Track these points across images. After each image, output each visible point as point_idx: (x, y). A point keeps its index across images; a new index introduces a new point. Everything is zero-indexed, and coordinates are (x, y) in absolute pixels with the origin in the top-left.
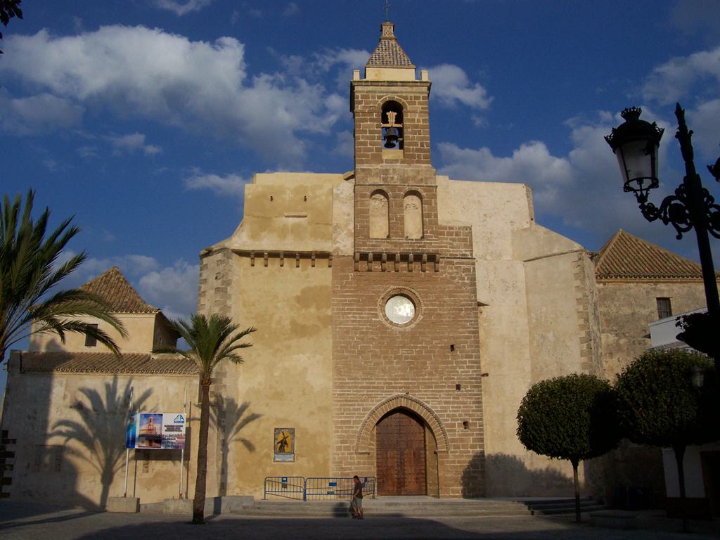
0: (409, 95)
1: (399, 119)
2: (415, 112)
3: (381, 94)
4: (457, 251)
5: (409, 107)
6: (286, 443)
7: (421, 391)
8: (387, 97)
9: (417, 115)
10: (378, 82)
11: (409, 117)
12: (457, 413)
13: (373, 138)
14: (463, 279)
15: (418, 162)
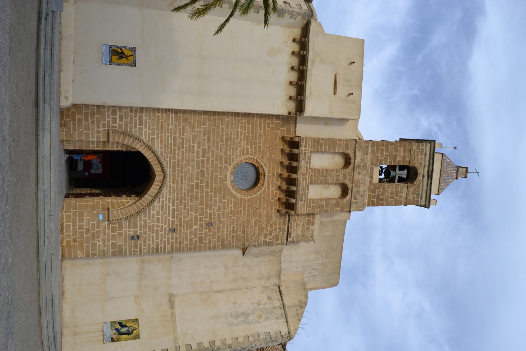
5: (411, 189)
6: (121, 58)
7: (170, 195)
8: (420, 171)
11: (404, 189)
12: (147, 229)
15: (370, 196)
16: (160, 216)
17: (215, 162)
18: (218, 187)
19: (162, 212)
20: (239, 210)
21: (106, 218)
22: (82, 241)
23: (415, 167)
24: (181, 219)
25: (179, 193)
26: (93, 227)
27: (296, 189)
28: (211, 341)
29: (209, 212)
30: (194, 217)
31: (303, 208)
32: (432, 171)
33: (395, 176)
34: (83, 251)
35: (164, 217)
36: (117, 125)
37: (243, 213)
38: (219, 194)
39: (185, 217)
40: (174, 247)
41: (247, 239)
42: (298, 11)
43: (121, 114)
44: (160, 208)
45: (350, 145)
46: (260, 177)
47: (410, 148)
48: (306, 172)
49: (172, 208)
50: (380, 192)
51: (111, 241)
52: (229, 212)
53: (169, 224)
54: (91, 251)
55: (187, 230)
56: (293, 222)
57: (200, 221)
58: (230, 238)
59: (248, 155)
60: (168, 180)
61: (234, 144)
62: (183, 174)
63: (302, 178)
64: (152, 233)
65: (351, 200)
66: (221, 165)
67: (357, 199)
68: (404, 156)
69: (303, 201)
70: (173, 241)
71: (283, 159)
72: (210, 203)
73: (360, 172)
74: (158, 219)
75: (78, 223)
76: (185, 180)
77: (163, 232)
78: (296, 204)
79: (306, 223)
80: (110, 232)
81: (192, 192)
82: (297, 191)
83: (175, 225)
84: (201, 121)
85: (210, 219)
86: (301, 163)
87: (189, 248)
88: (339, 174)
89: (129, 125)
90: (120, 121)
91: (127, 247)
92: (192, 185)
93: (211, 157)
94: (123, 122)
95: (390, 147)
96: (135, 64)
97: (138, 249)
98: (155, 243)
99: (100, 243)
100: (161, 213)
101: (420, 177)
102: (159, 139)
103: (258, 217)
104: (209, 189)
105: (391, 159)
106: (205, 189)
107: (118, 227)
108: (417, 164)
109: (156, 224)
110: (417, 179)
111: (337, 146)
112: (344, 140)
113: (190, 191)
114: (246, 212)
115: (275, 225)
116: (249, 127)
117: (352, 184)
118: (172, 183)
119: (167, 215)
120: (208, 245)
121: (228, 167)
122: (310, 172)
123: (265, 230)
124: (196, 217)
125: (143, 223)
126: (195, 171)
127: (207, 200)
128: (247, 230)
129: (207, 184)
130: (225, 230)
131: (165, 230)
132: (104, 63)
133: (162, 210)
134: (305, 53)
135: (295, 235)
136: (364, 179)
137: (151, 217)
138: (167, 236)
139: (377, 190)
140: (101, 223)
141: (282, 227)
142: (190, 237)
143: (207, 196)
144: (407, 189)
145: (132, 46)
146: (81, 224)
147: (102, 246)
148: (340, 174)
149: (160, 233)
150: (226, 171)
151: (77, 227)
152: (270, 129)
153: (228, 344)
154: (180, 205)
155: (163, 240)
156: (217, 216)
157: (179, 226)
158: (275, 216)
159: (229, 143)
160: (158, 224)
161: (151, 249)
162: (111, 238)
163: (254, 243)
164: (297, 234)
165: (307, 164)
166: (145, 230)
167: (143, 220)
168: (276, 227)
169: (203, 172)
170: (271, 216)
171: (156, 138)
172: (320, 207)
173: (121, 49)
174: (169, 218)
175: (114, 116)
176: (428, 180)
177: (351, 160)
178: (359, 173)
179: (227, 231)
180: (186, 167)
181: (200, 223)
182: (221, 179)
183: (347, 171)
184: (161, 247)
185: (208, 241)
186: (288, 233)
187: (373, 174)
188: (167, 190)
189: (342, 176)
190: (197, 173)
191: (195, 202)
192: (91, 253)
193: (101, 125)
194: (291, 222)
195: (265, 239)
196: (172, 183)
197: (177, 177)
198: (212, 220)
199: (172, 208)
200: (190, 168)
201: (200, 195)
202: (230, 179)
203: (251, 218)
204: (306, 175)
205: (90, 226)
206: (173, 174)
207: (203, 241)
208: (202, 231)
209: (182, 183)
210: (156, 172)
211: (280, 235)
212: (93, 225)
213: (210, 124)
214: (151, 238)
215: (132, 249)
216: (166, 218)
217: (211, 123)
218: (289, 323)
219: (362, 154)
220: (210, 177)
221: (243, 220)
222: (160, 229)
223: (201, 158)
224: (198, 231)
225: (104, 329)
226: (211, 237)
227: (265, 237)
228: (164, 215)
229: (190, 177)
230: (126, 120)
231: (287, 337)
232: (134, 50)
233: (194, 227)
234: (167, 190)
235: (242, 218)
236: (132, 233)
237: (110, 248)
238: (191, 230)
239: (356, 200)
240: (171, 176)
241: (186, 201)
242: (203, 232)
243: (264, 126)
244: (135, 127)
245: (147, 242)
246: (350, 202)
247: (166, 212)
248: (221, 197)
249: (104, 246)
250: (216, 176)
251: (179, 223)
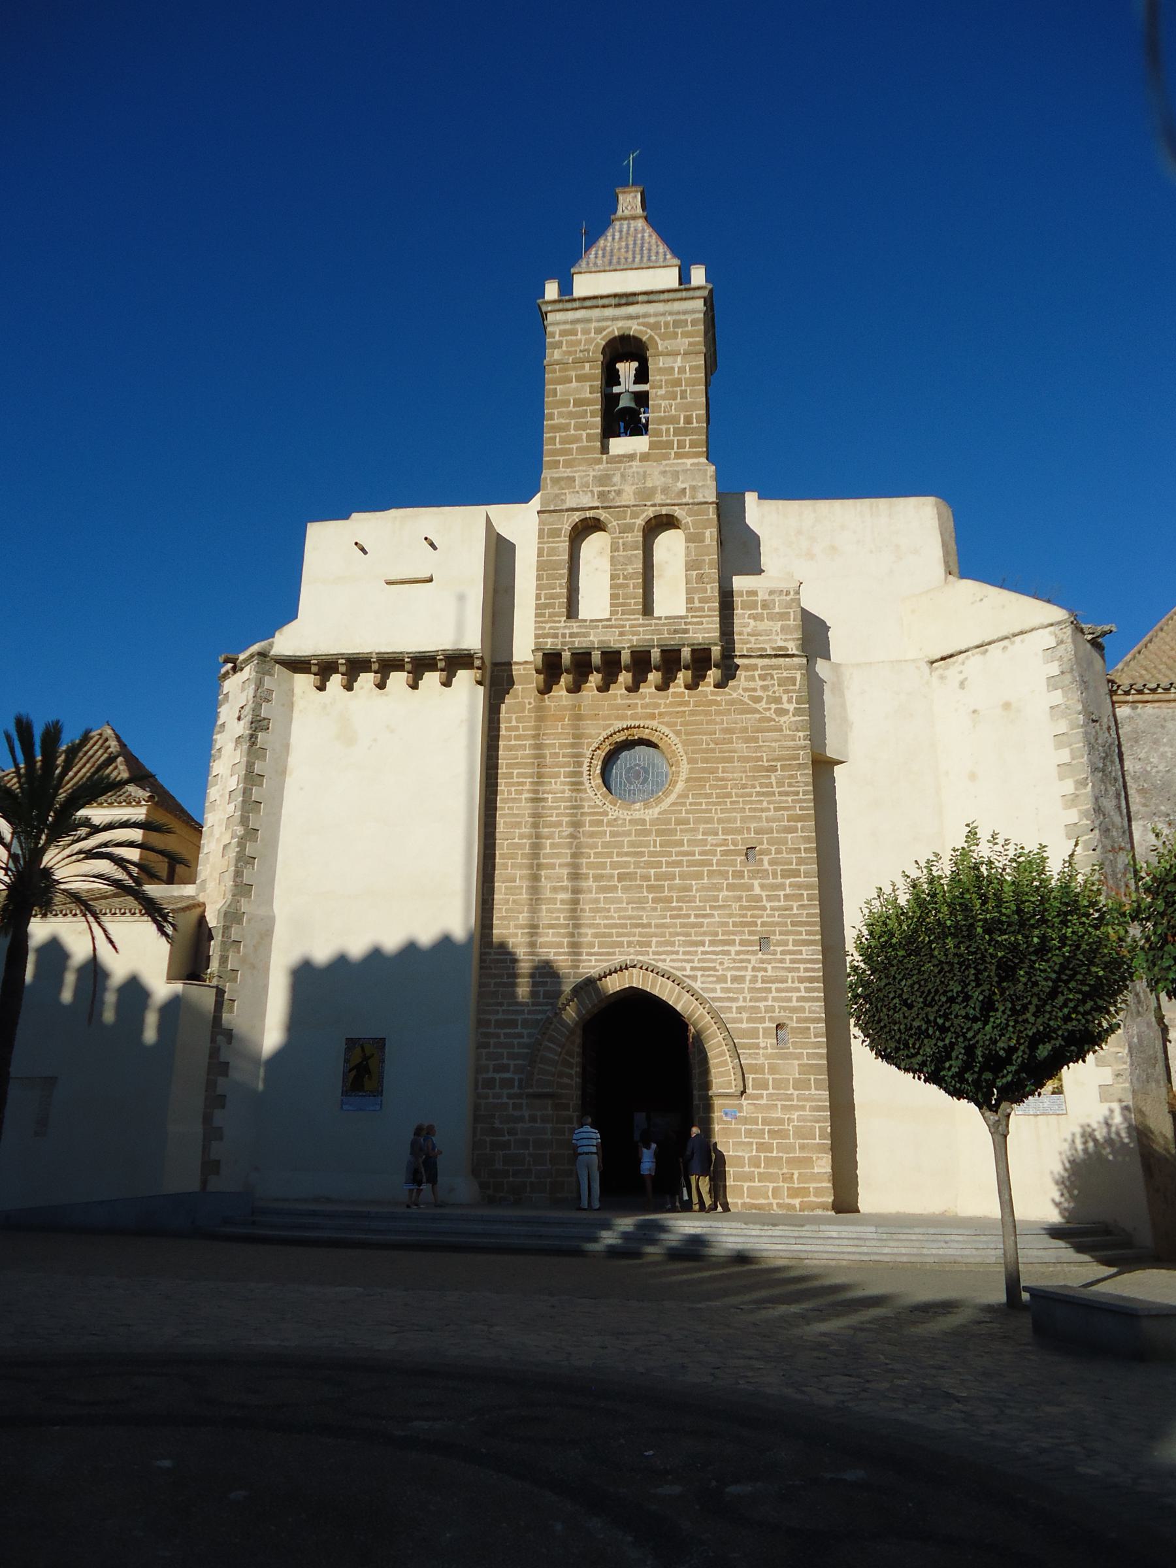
0: (662, 319)
1: (642, 376)
2: (675, 354)
3: (604, 324)
4: (764, 642)
5: (661, 345)
6: (367, 1070)
7: (677, 953)
8: (615, 329)
9: (679, 358)
10: (595, 298)
11: (661, 365)
12: (761, 1005)
13: (583, 415)
14: (778, 700)
15: (678, 456)
16: (729, 974)
17: (599, 850)
18: (658, 839)
19: (718, 971)
20: (715, 783)
21: (732, 1102)
22: (790, 1161)
23: (606, 344)
24: (735, 924)
25: (671, 930)
26: (754, 1133)
27: (656, 649)
28: (1067, 833)
29: (719, 857)
30: (730, 894)
31: (705, 626)
32: (615, 296)
33: (633, 393)
34: (814, 1159)
35: (731, 965)
36: (516, 1077)
37: (723, 772)
38: (676, 836)
39: (730, 916)
40: (807, 937)
41: (789, 759)
42: (253, 686)
43: (491, 1068)
44: (709, 976)
45: (551, 525)
46: (636, 737)
47: (557, 367)
48: (616, 627)
49: (709, 947)
50: (668, 430)
51: (789, 1092)
52: (719, 808)
53: (747, 952)
54: (815, 1139)
55: (764, 908)
56: (748, 646)
57: (743, 877)
58: (787, 802)
59: (582, 773)
60: (640, 958)
61: (558, 808)
62: (629, 922)
63: (630, 637)
64: (771, 992)
65: (685, 504)
66: (606, 833)
67: (685, 488)
68: (580, 379)
69: (687, 627)
70: (791, 940)
71: (592, 687)
72: (697, 855)
73: (615, 491)
74: (735, 979)
75: (745, 1169)
76: (641, 917)
77: (769, 967)
78: (693, 645)
79: (750, 612)
80: (768, 1092)
81: (669, 900)
82: (661, 646)
83: (752, 938)
84: (506, 888)
85: (736, 853)
86: (594, 642)
87: (809, 903)
88: (621, 544)
89: (516, 1050)
90: (508, 1071)
91: (805, 1052)
92: (655, 900)
93: (587, 858)
94: (509, 1065)
95: (556, 421)
96: (381, 1039)
97: (812, 1026)
98: (796, 984)
99: (794, 1119)
100: (720, 972)
101: (631, 328)
102: (547, 982)
103: (734, 736)
104: (664, 859)
105: (587, 413)
106: (664, 870)
107: (755, 1074)
108: (598, 340)
109: (748, 983)
110: (636, 335)
111: (554, 558)
112: (539, 543)
113: (667, 904)
114: (720, 765)
115: (755, 690)
116: (518, 773)
117: (646, 508)
118: (647, 949)
119: (726, 957)
120: (803, 855)
121: (610, 817)
122: (616, 617)
123: (768, 714)
124: (731, 887)
125: (745, 1015)
126: (620, 895)
127: (691, 864)
128: (765, 760)
129: (649, 865)
130: (764, 814)
131: (762, 961)
132: (378, 1108)
133: (714, 969)
134: (344, 661)
135: (780, 636)
136: (633, 477)
137: (731, 995)
138: (779, 956)
139: (664, 438)
140: (745, 1114)
141: (759, 672)
142: (782, 900)
143: (678, 864)
144: (661, 358)
145: (344, 1046)
146: (747, 1161)
147: (802, 1113)
148: (621, 541)
149: (769, 973)
150: (620, 822)
151: (754, 1171)
152: (521, 725)
153: (1076, 789)
154: (702, 926)
155: (788, 965)
156: (729, 837)
157: (754, 929)
158: (732, 692)
159: (554, 819)
160: (748, 978)
161: (812, 995)
162: (782, 1092)
163: (800, 740)
164: (779, 631)
165: (597, 627)
166: (763, 1010)
167: (739, 1015)
168: (758, 688)
169: (621, 878)
170: (732, 702)
171: (546, 989)
172: (703, 583)
173: (350, 1071)
174: (733, 953)
175: (497, 1084)
176: (637, 303)
177: (586, 518)
178: (619, 493)
179: (768, 810)
180: (612, 918)
181: (746, 877)
182: (639, 833)
183: (615, 523)
184: (806, 970)
185: (794, 856)
186: (776, 656)
187: (624, 456)
188: (664, 961)
189: (626, 535)
190: (625, 889)
191: (694, 891)
192: (820, 1139)
193: (517, 1113)
194: (747, 651)
195: (791, 713)
196: (647, 949)
197: (634, 936)
198: (740, 847)
199: (709, 947)
200: (612, 906)
201: (677, 881)
202: (639, 810)
203: (735, 752)
204: (623, 626)
205: (751, 1140)
206: (628, 948)
207: (794, 867)
208: (767, 870)
209: (649, 925)
210: (623, 987)
211: (779, 675)
212: (749, 1133)
213: (513, 866)
214: (783, 995)
215: (810, 1040)
216: (734, 961)
217: (510, 864)
218: (1027, 627)
219: (573, 492)
220: (634, 859)
221: (741, 772)
222: (760, 974)
223: (591, 883)
224: (769, 881)
225: (1031, 1113)
226: (784, 848)
227: (786, 712)
228: (726, 965)
229: (635, 906)
230: (505, 1057)
231: (1061, 629)
232: (351, 1043)
233: (757, 890)
234: (664, 961)
235: (735, 775)
236: (769, 1041)
237: (807, 1093)
238: (764, 898)
239: (687, 491)
240: (632, 950)
241: (693, 913)
242: (770, 868)
243: (515, 740)
244: (520, 1036)
245: (794, 1004)
246: (690, 506)
247: (719, 961)
248: (681, 830)
249: (803, 1108)
250: (632, 844)
251: (746, 929)
